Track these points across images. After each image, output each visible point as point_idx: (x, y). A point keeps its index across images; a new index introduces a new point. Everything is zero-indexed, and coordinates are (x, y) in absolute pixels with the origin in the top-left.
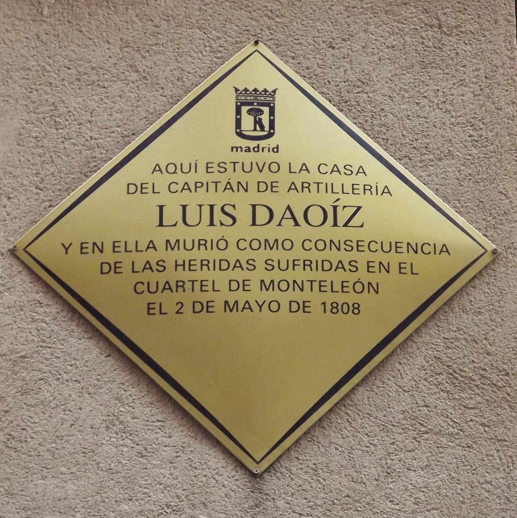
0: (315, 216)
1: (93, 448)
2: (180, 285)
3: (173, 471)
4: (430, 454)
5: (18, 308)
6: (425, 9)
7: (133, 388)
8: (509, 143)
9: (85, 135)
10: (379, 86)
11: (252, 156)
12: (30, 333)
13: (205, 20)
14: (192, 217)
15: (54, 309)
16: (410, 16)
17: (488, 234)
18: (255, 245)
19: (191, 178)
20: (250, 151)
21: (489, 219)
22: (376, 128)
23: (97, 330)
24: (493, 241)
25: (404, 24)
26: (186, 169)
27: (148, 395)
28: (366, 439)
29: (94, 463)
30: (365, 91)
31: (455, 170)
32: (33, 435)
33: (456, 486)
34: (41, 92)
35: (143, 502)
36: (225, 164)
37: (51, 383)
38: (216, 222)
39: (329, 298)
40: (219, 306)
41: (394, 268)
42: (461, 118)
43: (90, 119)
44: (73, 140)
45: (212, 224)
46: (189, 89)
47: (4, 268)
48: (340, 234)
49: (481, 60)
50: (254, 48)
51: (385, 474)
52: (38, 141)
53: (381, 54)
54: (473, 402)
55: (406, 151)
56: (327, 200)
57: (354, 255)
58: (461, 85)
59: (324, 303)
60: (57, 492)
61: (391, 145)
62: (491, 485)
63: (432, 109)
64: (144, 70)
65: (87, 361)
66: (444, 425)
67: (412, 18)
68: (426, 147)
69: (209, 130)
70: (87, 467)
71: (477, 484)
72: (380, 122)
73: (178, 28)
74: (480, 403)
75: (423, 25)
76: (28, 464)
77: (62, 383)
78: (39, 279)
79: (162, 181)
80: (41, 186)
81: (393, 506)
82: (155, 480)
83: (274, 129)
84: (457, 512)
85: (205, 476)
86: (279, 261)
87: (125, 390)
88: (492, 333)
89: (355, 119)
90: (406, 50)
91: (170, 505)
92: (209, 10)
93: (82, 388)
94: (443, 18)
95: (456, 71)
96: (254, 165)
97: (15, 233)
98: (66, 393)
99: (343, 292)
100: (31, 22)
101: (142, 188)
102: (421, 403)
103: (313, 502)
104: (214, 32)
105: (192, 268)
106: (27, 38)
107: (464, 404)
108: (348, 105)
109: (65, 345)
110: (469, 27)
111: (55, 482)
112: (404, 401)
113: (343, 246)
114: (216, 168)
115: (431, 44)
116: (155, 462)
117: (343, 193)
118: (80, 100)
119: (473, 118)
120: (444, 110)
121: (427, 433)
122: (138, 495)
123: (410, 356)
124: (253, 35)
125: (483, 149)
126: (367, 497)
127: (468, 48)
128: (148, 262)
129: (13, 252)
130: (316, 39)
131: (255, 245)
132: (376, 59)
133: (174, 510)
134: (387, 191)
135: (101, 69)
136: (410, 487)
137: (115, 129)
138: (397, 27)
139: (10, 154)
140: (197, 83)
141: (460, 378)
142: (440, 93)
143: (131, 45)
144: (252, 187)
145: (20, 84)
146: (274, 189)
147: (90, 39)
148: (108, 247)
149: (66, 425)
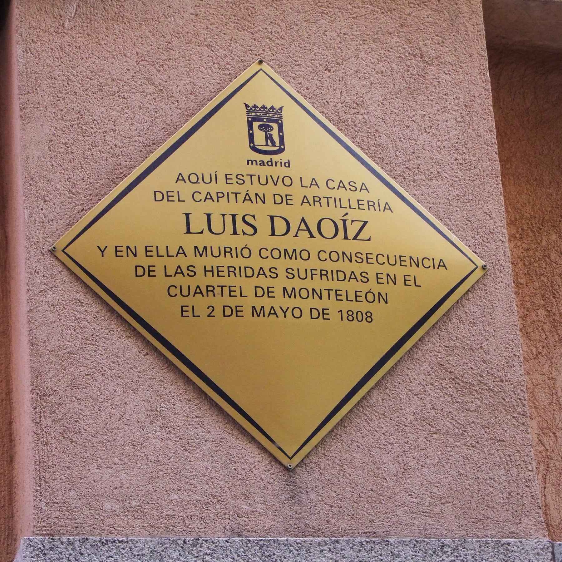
0: (328, 229)
1: (141, 440)
2: (210, 289)
3: (214, 464)
4: (440, 453)
5: (62, 306)
6: (408, 40)
7: (171, 385)
8: (490, 168)
9: (109, 143)
10: (372, 108)
11: (264, 171)
12: (74, 331)
13: (213, 38)
14: (217, 226)
15: (95, 307)
16: (395, 45)
17: (477, 251)
18: (276, 254)
19: (213, 189)
20: (264, 165)
21: (478, 237)
22: (373, 148)
23: (135, 329)
24: (482, 258)
25: (390, 52)
26: (207, 180)
27: (186, 392)
28: (383, 437)
29: (143, 454)
30: (361, 113)
31: (444, 190)
32: (86, 427)
33: (464, 482)
34: (67, 100)
35: (190, 493)
36: (243, 176)
37: (97, 378)
38: (239, 231)
39: (345, 306)
40: (247, 311)
41: (400, 280)
42: (447, 142)
43: (114, 128)
44: (100, 147)
45: (235, 233)
46: (202, 103)
47: (46, 268)
48: (351, 247)
49: (460, 89)
50: (259, 67)
51: (403, 470)
52: (68, 147)
53: (372, 78)
54: (473, 405)
55: (401, 170)
56: (337, 215)
57: (365, 267)
58: (445, 112)
59: (341, 311)
60: (112, 481)
61: (387, 164)
62: (494, 481)
63: (420, 133)
64: (160, 84)
65: (128, 359)
66: (451, 426)
67: (397, 47)
68: (418, 168)
69: (223, 144)
70: (137, 459)
71: (482, 480)
72: (375, 142)
73: (188, 45)
74: (480, 407)
75: (407, 54)
76: (84, 454)
77: (107, 379)
78: (78, 279)
79: (186, 189)
80: (74, 190)
81: (412, 500)
82: (199, 472)
83: (284, 145)
84: (467, 506)
85: (244, 469)
86: (298, 269)
87: (165, 388)
88: (486, 342)
89: (353, 138)
90: (394, 77)
91: (215, 496)
92: (215, 30)
93: (126, 385)
94: (424, 49)
95: (439, 98)
96: (269, 178)
97: (52, 235)
98: (111, 388)
99: (356, 301)
100: (54, 34)
101: (167, 196)
102: (429, 406)
103: (342, 495)
104: (221, 51)
105: (220, 274)
106: (52, 49)
107: (466, 407)
108: (346, 125)
109: (107, 342)
110: (447, 58)
111: (110, 472)
112: (414, 404)
113: (354, 258)
114: (235, 180)
115: (415, 73)
116: (197, 456)
117: (350, 208)
118: (104, 109)
119: (457, 143)
120: (431, 134)
121: (436, 433)
122: (185, 485)
123: (416, 362)
124: (256, 55)
125: (468, 172)
126: (389, 491)
127: (448, 78)
128: (179, 267)
129: (52, 252)
130: (313, 61)
131: (276, 254)
132: (368, 84)
133: (219, 500)
134: (387, 207)
135: (121, 80)
136: (425, 482)
137: (137, 138)
138: (385, 54)
139: (43, 159)
140: (209, 98)
141: (461, 383)
142: (427, 118)
143: (146, 59)
144: (269, 199)
145: (48, 92)
146: (289, 202)
147: (109, 52)
148: (141, 251)
149: (114, 419)
